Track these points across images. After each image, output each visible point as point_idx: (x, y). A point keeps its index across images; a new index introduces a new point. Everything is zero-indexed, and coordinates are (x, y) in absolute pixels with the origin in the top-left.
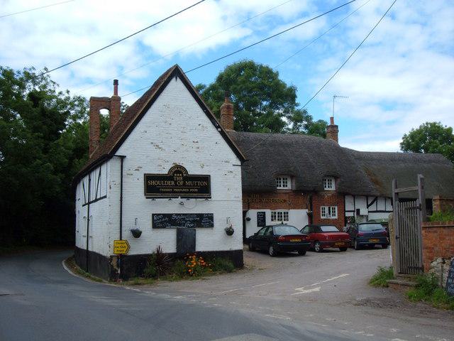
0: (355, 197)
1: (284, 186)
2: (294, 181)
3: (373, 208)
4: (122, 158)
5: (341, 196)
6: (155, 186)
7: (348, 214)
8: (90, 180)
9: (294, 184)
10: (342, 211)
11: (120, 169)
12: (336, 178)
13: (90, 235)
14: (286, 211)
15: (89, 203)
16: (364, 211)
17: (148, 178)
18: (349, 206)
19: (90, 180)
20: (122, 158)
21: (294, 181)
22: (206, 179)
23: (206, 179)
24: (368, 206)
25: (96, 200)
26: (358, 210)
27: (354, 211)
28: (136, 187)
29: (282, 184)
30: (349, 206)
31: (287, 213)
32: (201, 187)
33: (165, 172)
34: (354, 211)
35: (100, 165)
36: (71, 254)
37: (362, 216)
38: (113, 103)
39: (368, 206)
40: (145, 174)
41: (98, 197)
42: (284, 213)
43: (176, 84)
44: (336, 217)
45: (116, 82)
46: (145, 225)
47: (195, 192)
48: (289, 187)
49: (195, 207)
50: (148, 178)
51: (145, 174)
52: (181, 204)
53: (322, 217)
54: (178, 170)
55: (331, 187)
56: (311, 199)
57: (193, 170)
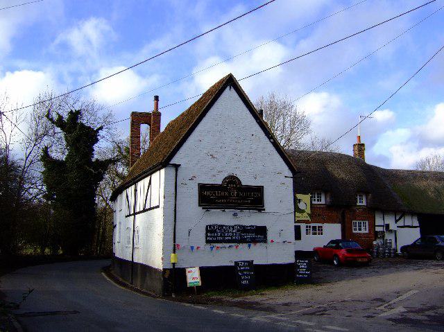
0: (385, 212)
1: (318, 200)
2: (328, 195)
3: (401, 223)
4: (177, 167)
5: (370, 213)
6: (211, 196)
7: (378, 229)
8: (136, 190)
9: (328, 199)
10: (372, 226)
11: (174, 178)
12: (367, 194)
13: (135, 246)
14: (320, 225)
15: (135, 214)
16: (393, 226)
17: (203, 188)
18: (379, 221)
19: (136, 190)
20: (177, 167)
21: (328, 195)
22: (260, 189)
23: (260, 189)
24: (396, 221)
25: (145, 210)
26: (387, 226)
27: (383, 226)
28: (191, 195)
29: (316, 199)
30: (379, 221)
31: (321, 227)
32: (253, 198)
33: (219, 182)
34: (383, 226)
35: (151, 174)
36: (107, 263)
37: (391, 231)
38: (152, 118)
39: (396, 221)
40: (199, 184)
41: (147, 207)
42: (319, 227)
43: (229, 93)
44: (367, 231)
45: (157, 98)
46: (200, 237)
47: (247, 203)
48: (323, 202)
49: (249, 219)
50: (203, 188)
51: (199, 184)
52: (235, 215)
53: (354, 232)
54: (232, 180)
55: (362, 202)
56: (343, 213)
57: (246, 181)
